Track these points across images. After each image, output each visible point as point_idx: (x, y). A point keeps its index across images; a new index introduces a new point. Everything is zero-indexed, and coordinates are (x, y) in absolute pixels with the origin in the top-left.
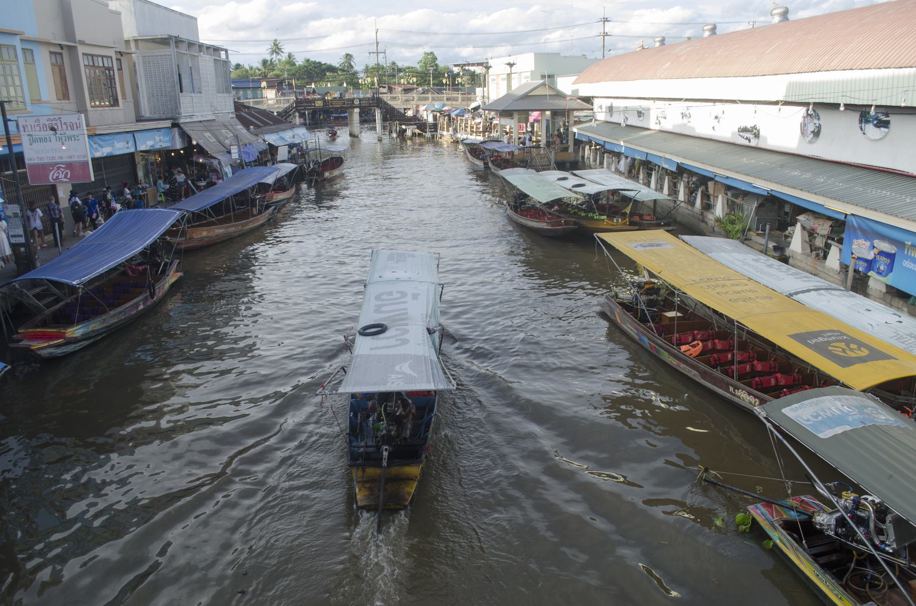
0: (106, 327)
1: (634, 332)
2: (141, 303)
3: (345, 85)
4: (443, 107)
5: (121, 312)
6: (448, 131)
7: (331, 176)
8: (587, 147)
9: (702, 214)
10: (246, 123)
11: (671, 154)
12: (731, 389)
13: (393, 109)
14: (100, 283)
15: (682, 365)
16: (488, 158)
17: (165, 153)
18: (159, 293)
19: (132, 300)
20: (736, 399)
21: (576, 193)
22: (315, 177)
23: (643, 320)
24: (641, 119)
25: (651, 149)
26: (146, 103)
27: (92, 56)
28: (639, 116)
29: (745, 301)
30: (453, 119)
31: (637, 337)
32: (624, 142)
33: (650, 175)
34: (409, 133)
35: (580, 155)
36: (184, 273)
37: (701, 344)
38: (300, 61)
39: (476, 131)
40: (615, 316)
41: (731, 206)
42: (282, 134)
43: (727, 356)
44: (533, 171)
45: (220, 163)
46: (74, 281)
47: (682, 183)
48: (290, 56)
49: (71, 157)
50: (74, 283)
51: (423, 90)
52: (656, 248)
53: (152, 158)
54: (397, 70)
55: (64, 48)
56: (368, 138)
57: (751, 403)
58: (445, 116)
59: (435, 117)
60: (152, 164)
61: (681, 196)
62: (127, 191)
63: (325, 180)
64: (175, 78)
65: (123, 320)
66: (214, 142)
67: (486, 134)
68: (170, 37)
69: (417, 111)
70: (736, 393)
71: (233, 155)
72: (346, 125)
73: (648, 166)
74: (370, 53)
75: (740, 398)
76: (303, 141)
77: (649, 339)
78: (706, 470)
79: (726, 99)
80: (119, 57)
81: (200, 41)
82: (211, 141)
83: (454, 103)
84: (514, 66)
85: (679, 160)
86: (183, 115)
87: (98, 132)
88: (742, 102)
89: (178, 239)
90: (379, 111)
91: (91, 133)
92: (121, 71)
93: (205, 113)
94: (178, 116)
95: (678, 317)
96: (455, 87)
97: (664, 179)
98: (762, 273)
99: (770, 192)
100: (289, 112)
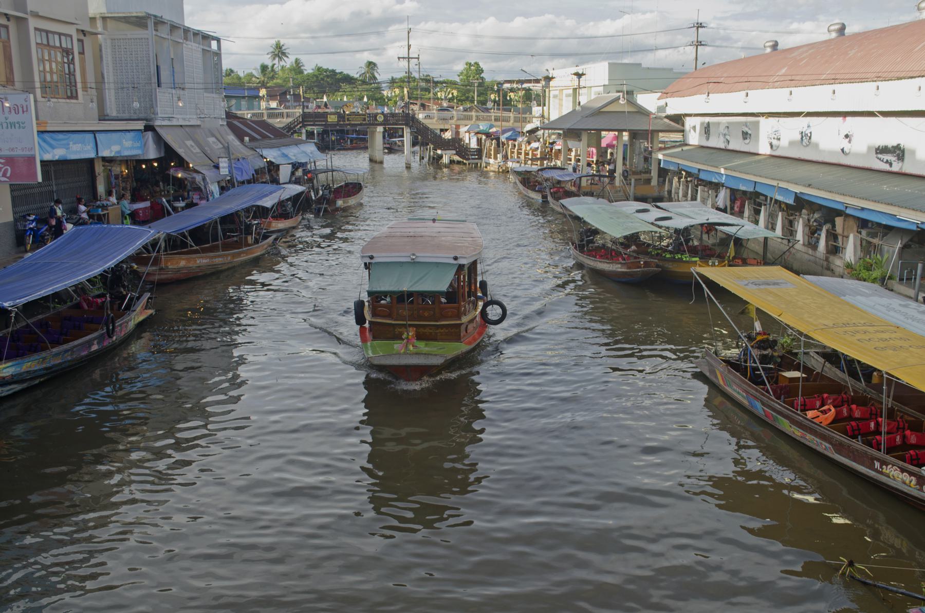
0: (45, 369)
1: (743, 396)
2: (95, 342)
3: (365, 99)
4: (489, 129)
5: (66, 351)
6: (496, 158)
7: (346, 205)
8: (676, 179)
9: (827, 259)
10: (240, 135)
11: (788, 182)
12: (877, 465)
13: (426, 129)
14: (44, 316)
15: (809, 436)
16: (547, 190)
17: (135, 163)
18: (121, 332)
19: (84, 336)
20: (883, 479)
21: (660, 227)
22: (324, 206)
23: (756, 380)
24: (747, 141)
25: (760, 176)
26: (113, 99)
27: (47, 32)
28: (745, 138)
29: (895, 350)
30: (503, 144)
31: (745, 402)
32: (725, 169)
33: (757, 212)
34: (445, 160)
35: (666, 189)
36: (156, 311)
37: (833, 410)
38: (309, 68)
39: (532, 158)
40: (716, 377)
41: (866, 248)
42: (285, 150)
43: (869, 425)
44: (605, 201)
45: (204, 179)
46: (5, 302)
47: (801, 219)
48: (297, 61)
49: (12, 150)
50: (6, 304)
51: (464, 108)
52: (771, 286)
53: (116, 170)
54: (430, 83)
55: (11, 19)
56: (393, 163)
57: (904, 483)
58: (492, 140)
59: (479, 141)
60: (117, 177)
61: (800, 236)
62: (82, 208)
63: (337, 209)
64: (152, 69)
65: (69, 361)
66: (197, 153)
67: (545, 162)
68: (148, 16)
69: (457, 133)
70: (884, 470)
71: (221, 170)
72: (366, 148)
73: (755, 201)
74: (399, 58)
75: (889, 477)
76: (312, 160)
77: (763, 404)
78: (851, 564)
79: (860, 110)
80: (82, 37)
81: (186, 25)
82: (195, 151)
83: (504, 124)
84: (583, 77)
85: (798, 189)
86: (160, 115)
87: (49, 129)
88: (886, 114)
89: (149, 269)
90: (409, 130)
91: (42, 129)
92: (83, 56)
93: (188, 116)
94: (153, 116)
95: (803, 378)
96: (505, 104)
97: (777, 216)
98: (913, 321)
99: (920, 226)
100: (294, 127)
